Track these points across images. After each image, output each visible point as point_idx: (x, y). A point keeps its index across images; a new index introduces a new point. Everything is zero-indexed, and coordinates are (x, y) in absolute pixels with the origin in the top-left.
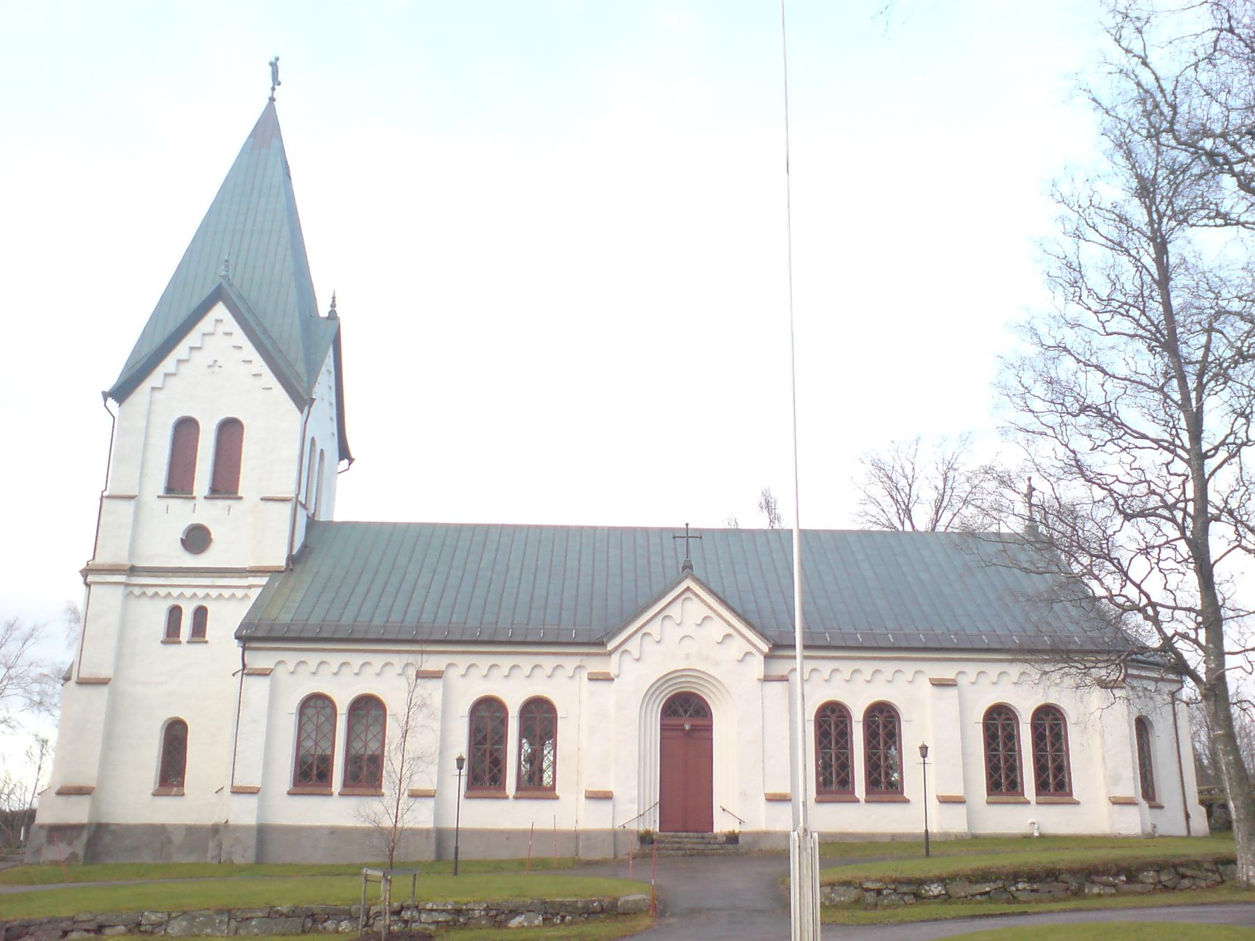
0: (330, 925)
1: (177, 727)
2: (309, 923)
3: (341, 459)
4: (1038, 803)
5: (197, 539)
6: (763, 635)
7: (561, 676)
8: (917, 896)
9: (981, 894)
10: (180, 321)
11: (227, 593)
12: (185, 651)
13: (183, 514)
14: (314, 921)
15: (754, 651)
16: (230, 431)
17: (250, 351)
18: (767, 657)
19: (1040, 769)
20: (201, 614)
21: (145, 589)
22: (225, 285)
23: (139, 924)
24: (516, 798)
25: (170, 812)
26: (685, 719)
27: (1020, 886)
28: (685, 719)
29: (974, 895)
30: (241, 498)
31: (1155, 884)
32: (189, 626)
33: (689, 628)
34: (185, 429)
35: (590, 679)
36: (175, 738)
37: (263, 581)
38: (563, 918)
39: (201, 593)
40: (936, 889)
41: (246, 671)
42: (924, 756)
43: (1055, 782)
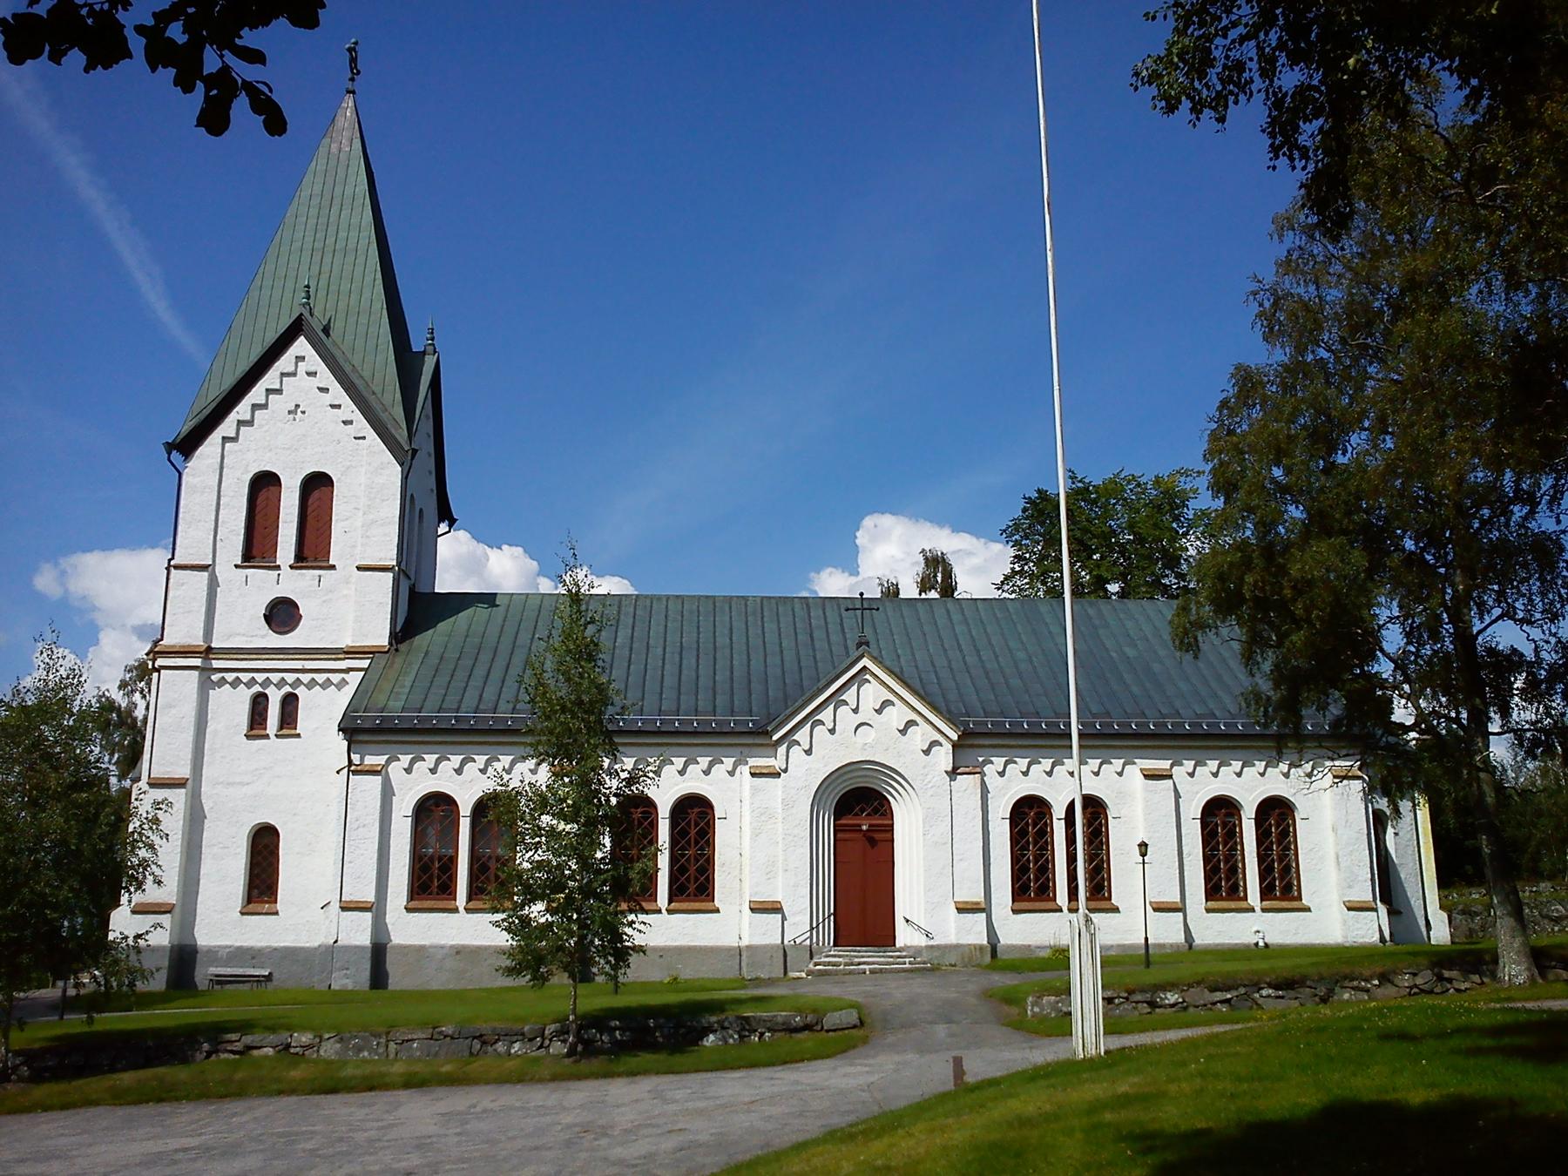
0: (501, 1047)
1: (637, 814)
2: (477, 1045)
3: (441, 520)
4: (1264, 910)
5: (282, 614)
6: (951, 720)
7: (720, 771)
8: (1152, 1004)
9: (1222, 1002)
10: (254, 358)
11: (321, 678)
12: (273, 747)
13: (264, 586)
14: (484, 1043)
15: (941, 739)
16: (317, 485)
17: (338, 393)
18: (955, 746)
19: (1265, 872)
20: (290, 702)
21: (240, 675)
22: (306, 314)
23: (288, 1046)
24: (670, 912)
25: (260, 933)
26: (858, 814)
27: (1264, 992)
28: (858, 814)
29: (1214, 1004)
30: (333, 567)
31: (1411, 988)
32: (272, 717)
33: (866, 713)
34: (264, 483)
35: (753, 775)
36: (264, 843)
37: (365, 664)
38: (762, 1034)
39: (290, 678)
40: (1172, 998)
41: (353, 770)
42: (1143, 855)
43: (1282, 885)
